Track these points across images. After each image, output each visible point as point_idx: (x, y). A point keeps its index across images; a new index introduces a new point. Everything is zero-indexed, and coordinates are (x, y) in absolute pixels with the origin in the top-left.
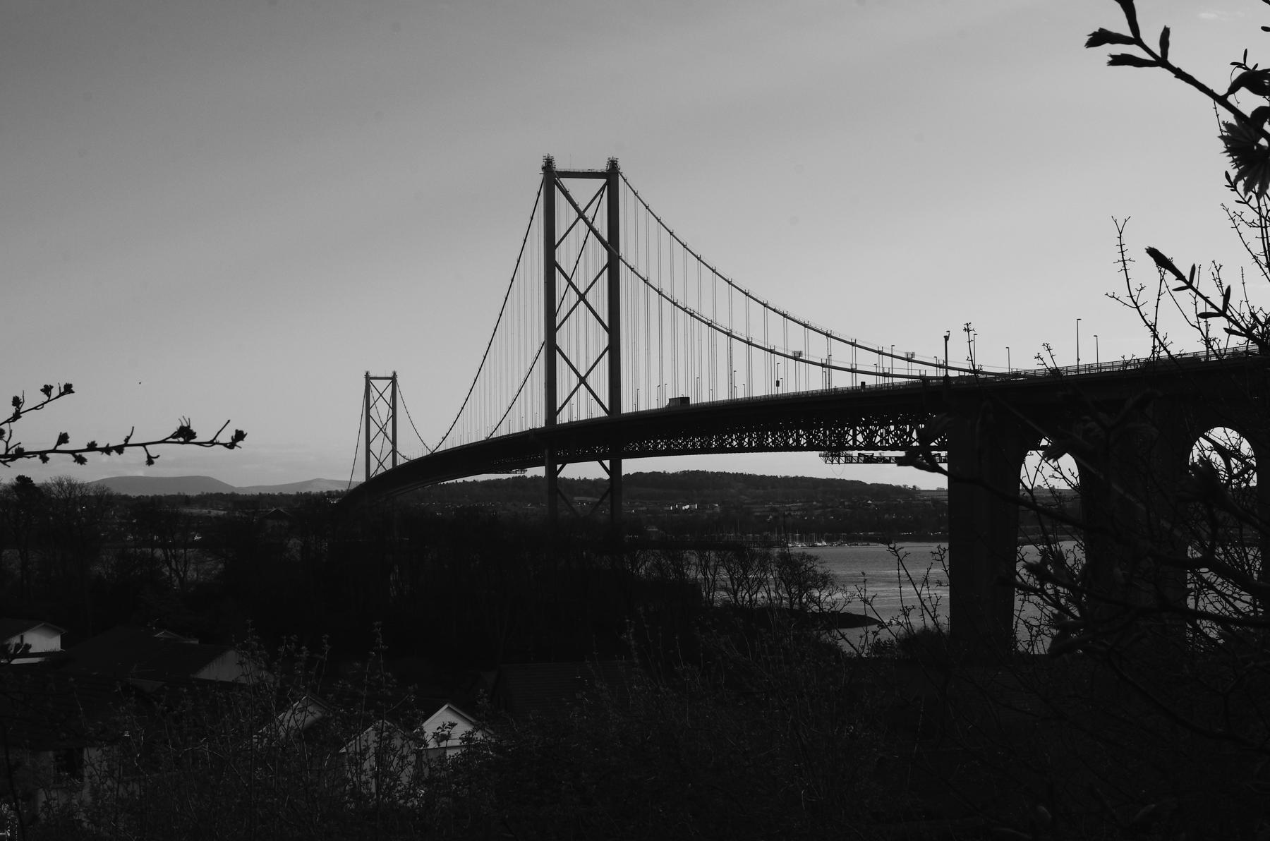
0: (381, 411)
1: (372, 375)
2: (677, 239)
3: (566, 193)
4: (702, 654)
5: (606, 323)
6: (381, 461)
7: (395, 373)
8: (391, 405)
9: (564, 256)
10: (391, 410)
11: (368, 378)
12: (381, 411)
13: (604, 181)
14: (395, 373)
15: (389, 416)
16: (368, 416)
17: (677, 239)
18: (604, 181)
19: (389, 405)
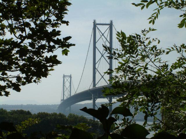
0: (67, 84)
1: (97, 22)
2: (100, 52)
3: (98, 28)
4: (184, 90)
5: (96, 49)
6: (103, 54)
7: (111, 22)
8: (96, 70)
9: (69, 84)
10: (96, 67)
11: (95, 25)
12: (67, 84)
13: (109, 26)
14: (111, 22)
15: (138, 66)
16: (64, 94)
17: (100, 52)
18: (109, 26)
19: (97, 70)
